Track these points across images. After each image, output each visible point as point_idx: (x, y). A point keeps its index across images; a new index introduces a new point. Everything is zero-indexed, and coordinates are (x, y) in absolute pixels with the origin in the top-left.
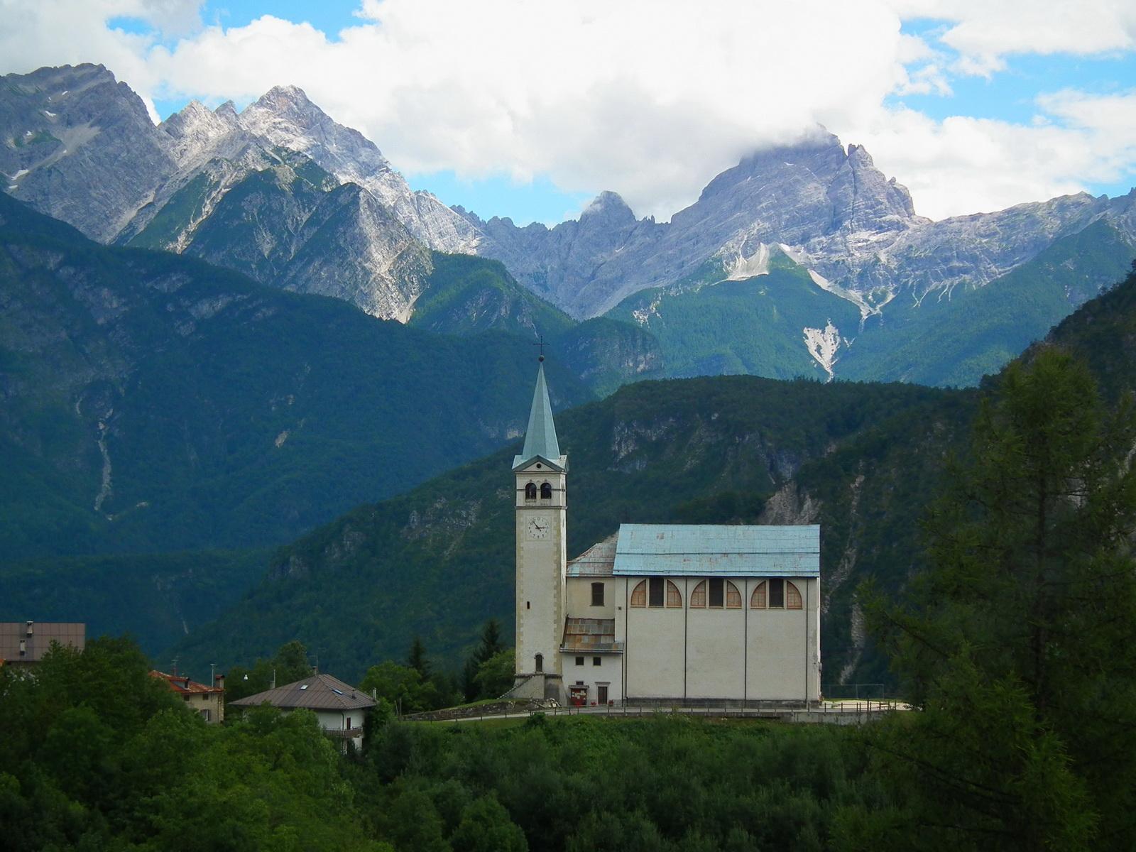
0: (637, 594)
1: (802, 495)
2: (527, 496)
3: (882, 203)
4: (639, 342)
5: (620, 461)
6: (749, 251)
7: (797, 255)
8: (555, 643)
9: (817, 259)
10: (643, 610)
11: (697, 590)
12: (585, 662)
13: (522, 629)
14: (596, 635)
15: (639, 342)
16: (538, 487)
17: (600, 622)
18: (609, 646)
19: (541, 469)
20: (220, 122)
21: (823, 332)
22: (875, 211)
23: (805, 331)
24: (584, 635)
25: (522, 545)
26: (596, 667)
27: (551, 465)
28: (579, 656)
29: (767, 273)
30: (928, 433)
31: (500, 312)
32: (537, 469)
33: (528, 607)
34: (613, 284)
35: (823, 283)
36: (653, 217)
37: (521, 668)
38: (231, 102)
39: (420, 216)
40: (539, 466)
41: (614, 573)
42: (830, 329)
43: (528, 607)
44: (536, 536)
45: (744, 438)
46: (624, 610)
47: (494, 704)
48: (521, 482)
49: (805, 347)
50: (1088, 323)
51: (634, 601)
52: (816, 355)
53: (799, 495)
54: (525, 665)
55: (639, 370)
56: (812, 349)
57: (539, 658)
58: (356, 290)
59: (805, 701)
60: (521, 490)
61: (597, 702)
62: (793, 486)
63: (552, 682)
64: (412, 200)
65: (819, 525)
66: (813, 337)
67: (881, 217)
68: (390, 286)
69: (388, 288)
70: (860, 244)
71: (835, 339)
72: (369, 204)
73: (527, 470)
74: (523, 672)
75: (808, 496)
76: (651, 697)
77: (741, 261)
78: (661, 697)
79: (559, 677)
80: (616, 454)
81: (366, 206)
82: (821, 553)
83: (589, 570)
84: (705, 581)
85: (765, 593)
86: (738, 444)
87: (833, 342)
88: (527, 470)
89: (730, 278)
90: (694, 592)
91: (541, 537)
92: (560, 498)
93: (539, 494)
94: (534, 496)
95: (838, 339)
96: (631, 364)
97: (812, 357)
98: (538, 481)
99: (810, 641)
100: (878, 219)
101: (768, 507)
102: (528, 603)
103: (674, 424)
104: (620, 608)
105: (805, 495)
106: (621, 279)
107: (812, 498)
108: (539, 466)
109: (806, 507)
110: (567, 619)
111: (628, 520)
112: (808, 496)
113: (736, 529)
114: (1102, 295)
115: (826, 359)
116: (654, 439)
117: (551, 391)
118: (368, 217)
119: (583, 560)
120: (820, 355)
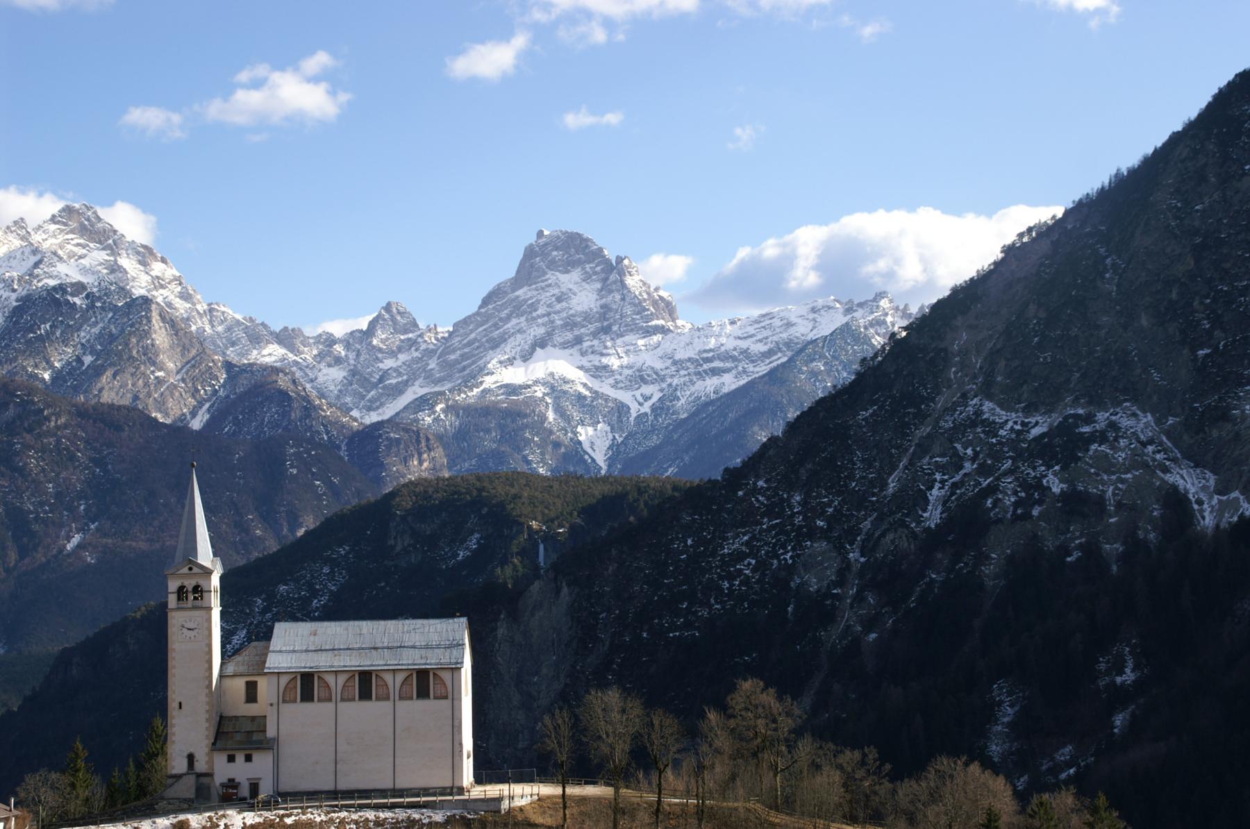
1: (559, 583)
2: (179, 599)
3: (648, 310)
4: (423, 444)
8: (207, 742)
10: (296, 704)
11: (347, 684)
12: (237, 759)
13: (174, 729)
14: (248, 732)
15: (423, 444)
17: (253, 718)
18: (261, 742)
19: (192, 572)
20: (10, 238)
22: (642, 317)
26: (248, 764)
28: (248, 752)
30: (675, 523)
31: (290, 416)
33: (180, 707)
34: (398, 390)
37: (173, 768)
38: (22, 219)
39: (213, 326)
40: (190, 569)
41: (265, 671)
43: (180, 707)
44: (188, 637)
46: (275, 707)
47: (143, 806)
51: (286, 698)
52: (590, 451)
54: (178, 765)
55: (423, 468)
57: (191, 758)
58: (150, 397)
59: (452, 788)
60: (173, 593)
61: (249, 798)
63: (204, 780)
64: (204, 311)
67: (647, 322)
68: (183, 394)
69: (181, 395)
72: (160, 315)
73: (178, 573)
74: (174, 772)
75: (564, 584)
76: (302, 790)
78: (312, 790)
79: (210, 775)
80: (393, 547)
81: (159, 318)
84: (354, 675)
87: (605, 438)
88: (178, 573)
90: (344, 686)
91: (192, 638)
96: (416, 463)
98: (190, 584)
99: (455, 729)
100: (645, 325)
102: (180, 704)
105: (561, 583)
106: (406, 384)
107: (569, 585)
108: (190, 569)
109: (562, 594)
110: (221, 717)
111: (279, 621)
112: (564, 584)
113: (386, 626)
114: (833, 392)
115: (600, 458)
117: (1086, 435)
118: (160, 328)
120: (594, 450)
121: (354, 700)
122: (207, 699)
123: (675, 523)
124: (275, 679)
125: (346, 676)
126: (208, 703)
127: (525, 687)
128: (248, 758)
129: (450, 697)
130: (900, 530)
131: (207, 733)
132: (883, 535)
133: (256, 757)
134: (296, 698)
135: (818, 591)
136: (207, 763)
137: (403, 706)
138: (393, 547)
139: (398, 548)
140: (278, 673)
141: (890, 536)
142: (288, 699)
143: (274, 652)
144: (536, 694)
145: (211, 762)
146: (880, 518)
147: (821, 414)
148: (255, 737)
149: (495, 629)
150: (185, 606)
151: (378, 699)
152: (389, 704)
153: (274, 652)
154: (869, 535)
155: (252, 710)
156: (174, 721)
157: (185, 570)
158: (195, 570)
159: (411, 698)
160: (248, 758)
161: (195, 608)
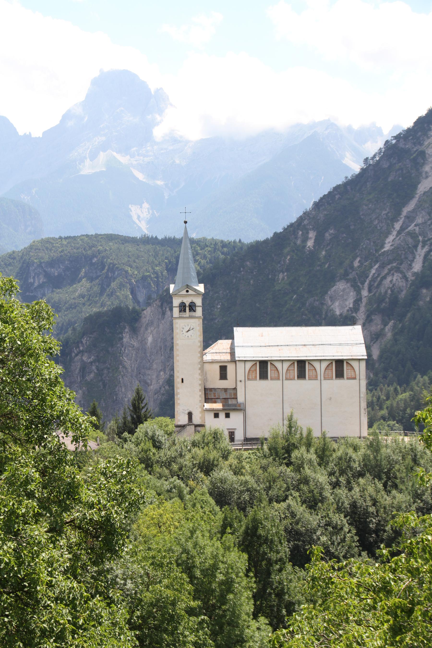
0: (251, 372)
5: (35, 288)
6: (94, 156)
7: (123, 159)
9: (136, 161)
13: (179, 396)
14: (225, 398)
16: (187, 304)
18: (235, 405)
21: (141, 207)
23: (130, 206)
24: (217, 398)
25: (178, 342)
26: (227, 419)
27: (195, 290)
28: (227, 412)
29: (104, 169)
30: (242, 269)
32: (186, 293)
33: (182, 382)
35: (140, 176)
36: (30, 133)
40: (187, 291)
42: (146, 205)
43: (182, 382)
44: (186, 337)
45: (114, 273)
46: (243, 382)
48: (176, 302)
49: (130, 217)
50: (336, 199)
51: (249, 377)
52: (137, 221)
53: (162, 309)
56: (135, 218)
57: (190, 415)
60: (176, 307)
62: (158, 303)
65: (235, 329)
66: (135, 211)
70: (162, 151)
71: (149, 212)
77: (88, 162)
80: (32, 284)
82: (365, 343)
83: (217, 357)
85: (332, 369)
86: (111, 277)
89: (82, 173)
90: (287, 370)
91: (190, 337)
92: (199, 311)
93: (187, 309)
94: (185, 311)
95: (151, 211)
97: (134, 223)
98: (187, 301)
101: (143, 316)
102: (182, 379)
103: (69, 265)
104: (241, 381)
105: (166, 308)
108: (187, 291)
110: (205, 389)
116: (56, 274)
119: (212, 351)
120: (140, 221)
121: (294, 379)
122: (200, 377)
123: (242, 269)
124: (242, 364)
125: (288, 364)
126: (201, 380)
127: (142, 376)
128: (227, 416)
129: (358, 377)
130: (396, 274)
131: (200, 399)
132: (384, 278)
133: (233, 415)
134: (256, 377)
135: (341, 315)
136: (201, 418)
137: (326, 384)
138: (32, 284)
139: (36, 284)
140: (245, 361)
141: (389, 279)
142: (251, 377)
143: (238, 346)
144: (149, 381)
145: (203, 418)
146: (382, 267)
147: (337, 197)
148: (230, 402)
149: (122, 339)
150: (185, 316)
151: (310, 379)
152: (317, 382)
153: (238, 346)
154: (374, 279)
155: (224, 384)
156: (178, 391)
157: (184, 292)
158: (191, 292)
159: (332, 379)
160: (227, 416)
161: (191, 317)
